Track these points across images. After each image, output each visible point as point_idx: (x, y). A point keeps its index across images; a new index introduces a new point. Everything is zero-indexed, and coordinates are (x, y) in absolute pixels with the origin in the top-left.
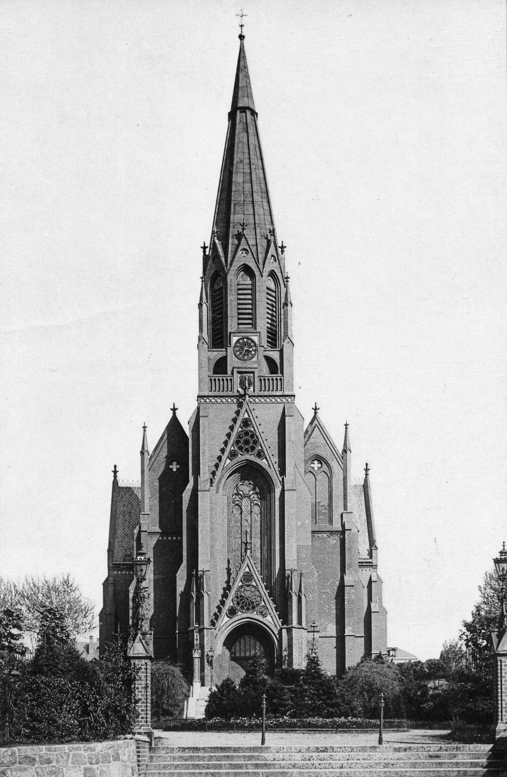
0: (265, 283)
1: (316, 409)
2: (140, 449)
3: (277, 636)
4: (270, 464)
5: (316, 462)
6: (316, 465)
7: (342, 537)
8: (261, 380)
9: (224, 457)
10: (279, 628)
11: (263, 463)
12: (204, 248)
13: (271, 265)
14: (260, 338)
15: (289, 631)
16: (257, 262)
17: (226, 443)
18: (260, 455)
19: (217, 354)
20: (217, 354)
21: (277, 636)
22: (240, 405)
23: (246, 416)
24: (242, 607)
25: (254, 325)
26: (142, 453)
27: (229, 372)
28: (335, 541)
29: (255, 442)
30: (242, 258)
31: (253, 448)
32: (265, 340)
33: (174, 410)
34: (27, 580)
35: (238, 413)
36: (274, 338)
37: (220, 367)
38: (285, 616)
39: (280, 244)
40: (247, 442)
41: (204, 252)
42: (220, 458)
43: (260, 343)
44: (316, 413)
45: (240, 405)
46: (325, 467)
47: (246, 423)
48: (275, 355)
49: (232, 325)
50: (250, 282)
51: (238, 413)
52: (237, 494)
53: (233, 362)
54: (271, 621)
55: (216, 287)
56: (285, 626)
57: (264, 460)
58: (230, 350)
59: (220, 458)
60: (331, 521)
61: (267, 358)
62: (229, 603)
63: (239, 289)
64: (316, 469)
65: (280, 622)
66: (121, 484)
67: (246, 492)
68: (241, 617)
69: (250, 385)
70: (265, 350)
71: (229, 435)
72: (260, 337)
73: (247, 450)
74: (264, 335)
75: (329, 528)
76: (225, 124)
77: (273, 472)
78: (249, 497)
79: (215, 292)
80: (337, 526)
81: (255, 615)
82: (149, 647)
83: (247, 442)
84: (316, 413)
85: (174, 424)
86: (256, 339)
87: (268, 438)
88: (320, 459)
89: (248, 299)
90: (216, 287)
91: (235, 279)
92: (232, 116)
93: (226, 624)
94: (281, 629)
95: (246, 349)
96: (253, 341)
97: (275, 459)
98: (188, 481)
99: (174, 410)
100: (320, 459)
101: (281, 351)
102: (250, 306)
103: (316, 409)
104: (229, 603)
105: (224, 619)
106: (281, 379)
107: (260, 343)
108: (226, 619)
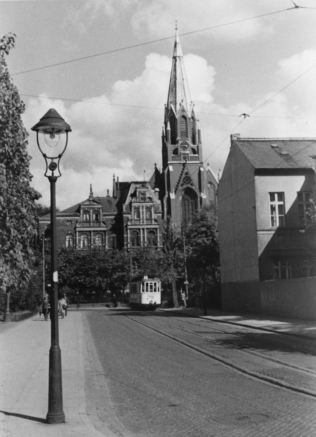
4: (195, 188)
6: (209, 185)
9: (179, 186)
12: (165, 105)
17: (179, 180)
18: (192, 185)
22: (184, 166)
23: (186, 171)
27: (179, 155)
29: (190, 180)
34: (180, 60)
35: (183, 169)
42: (177, 186)
45: (184, 166)
47: (187, 173)
50: (184, 120)
51: (183, 169)
53: (181, 151)
57: (194, 187)
59: (177, 186)
62: (181, 182)
63: (181, 132)
66: (44, 417)
71: (180, 178)
73: (187, 183)
77: (197, 191)
81: (189, 186)
83: (187, 180)
85: (157, 171)
87: (195, 178)
96: (187, 143)
97: (197, 186)
98: (165, 194)
104: (181, 182)
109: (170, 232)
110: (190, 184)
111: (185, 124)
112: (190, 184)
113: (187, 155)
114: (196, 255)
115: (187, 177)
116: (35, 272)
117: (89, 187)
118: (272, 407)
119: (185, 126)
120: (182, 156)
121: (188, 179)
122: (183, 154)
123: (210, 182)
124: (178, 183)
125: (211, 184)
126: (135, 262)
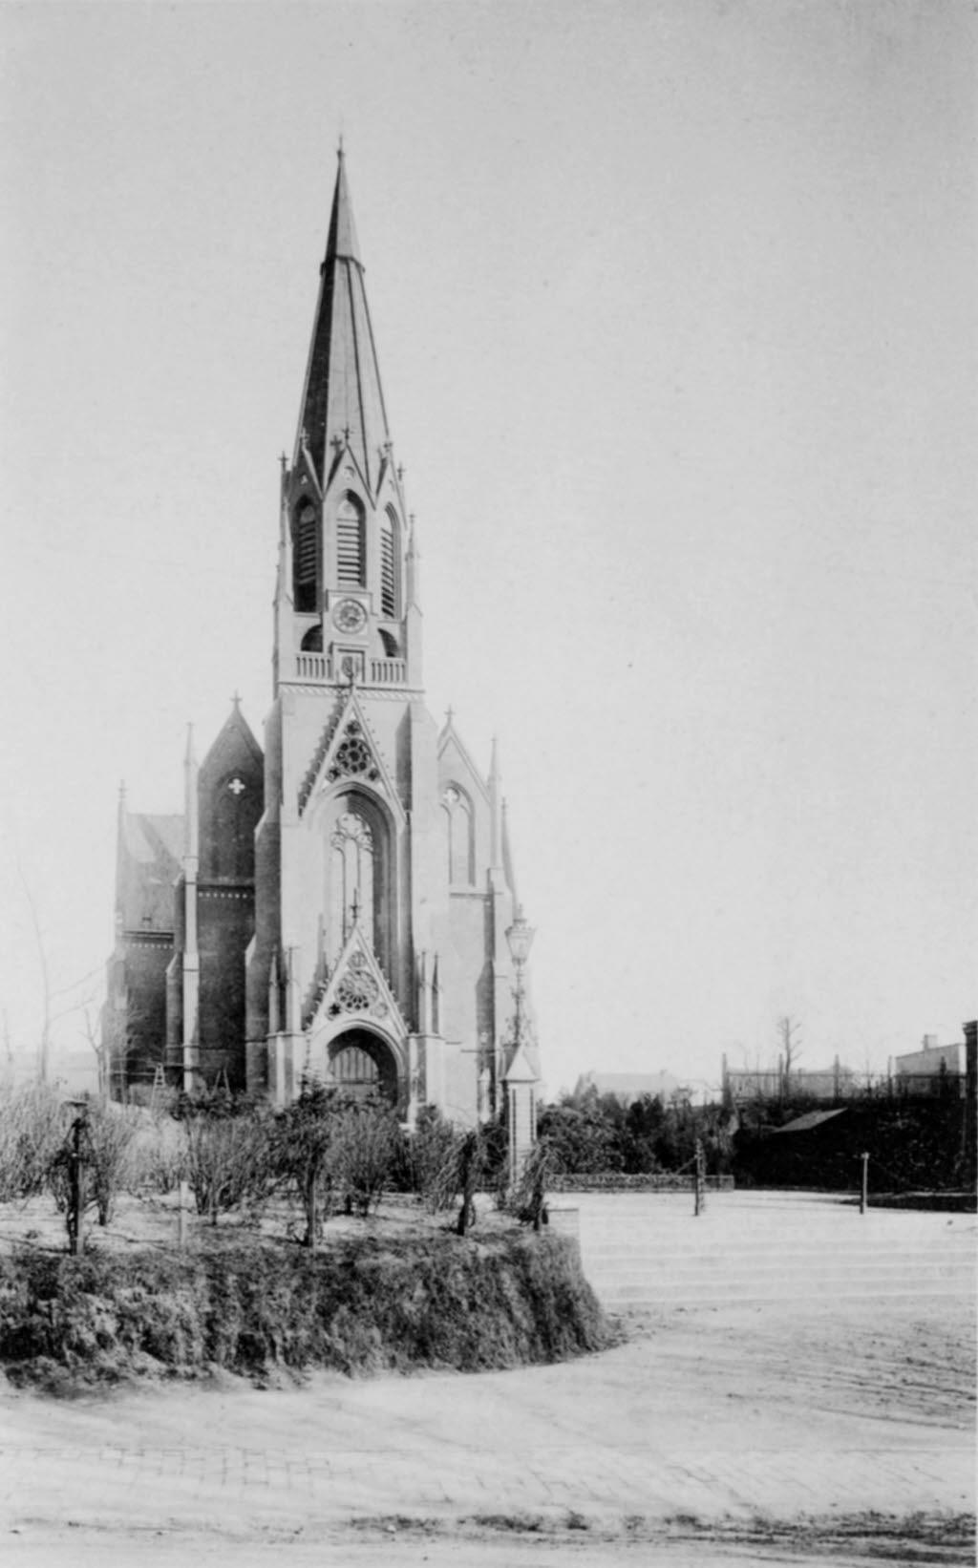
0: (378, 522)
1: (449, 713)
2: (321, 256)
3: (401, 1045)
4: (386, 789)
5: (450, 792)
6: (451, 795)
7: (488, 904)
8: (373, 665)
10: (403, 1035)
11: (378, 787)
12: (284, 460)
13: (387, 495)
14: (371, 600)
15: (421, 1045)
16: (367, 486)
19: (308, 621)
20: (308, 621)
21: (401, 1045)
23: (353, 717)
24: (349, 1005)
25: (362, 582)
26: (187, 763)
28: (478, 908)
30: (344, 480)
31: (363, 766)
32: (378, 606)
33: (237, 700)
36: (389, 603)
37: (312, 640)
38: (413, 1023)
39: (397, 467)
40: (354, 756)
41: (284, 465)
43: (371, 607)
44: (449, 719)
46: (463, 800)
48: (394, 630)
49: (330, 578)
52: (339, 833)
53: (330, 634)
54: (389, 1024)
55: (304, 520)
56: (413, 1034)
58: (327, 616)
60: (472, 880)
61: (382, 632)
64: (450, 801)
65: (406, 1030)
67: (351, 831)
68: (347, 1021)
69: (357, 670)
70: (378, 620)
72: (371, 599)
73: (355, 769)
74: (378, 599)
75: (471, 890)
76: (316, 281)
77: (395, 807)
78: (354, 839)
79: (301, 527)
80: (481, 887)
82: (194, 1081)
84: (449, 719)
86: (365, 602)
87: (385, 753)
88: (457, 788)
89: (353, 557)
90: (304, 520)
91: (335, 512)
92: (327, 269)
93: (326, 1028)
94: (408, 1038)
95: (351, 617)
99: (237, 700)
100: (457, 788)
101: (404, 623)
102: (356, 568)
103: (449, 713)
104: (330, 998)
105: (321, 1018)
106: (403, 666)
107: (371, 607)
108: (326, 783)
109: (659, 1168)
110: (367, 771)
111: (356, 546)
112: (367, 771)
113: (360, 655)
114: (911, 1145)
115: (353, 743)
116: (744, 1115)
117: (529, 1095)
118: (565, 1348)
119: (356, 539)
120: (338, 658)
121: (355, 754)
122: (341, 650)
123: (452, 782)
124: (317, 767)
125: (456, 792)
126: (847, 1131)
